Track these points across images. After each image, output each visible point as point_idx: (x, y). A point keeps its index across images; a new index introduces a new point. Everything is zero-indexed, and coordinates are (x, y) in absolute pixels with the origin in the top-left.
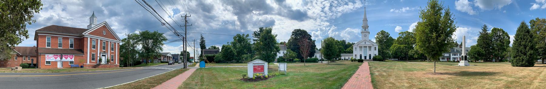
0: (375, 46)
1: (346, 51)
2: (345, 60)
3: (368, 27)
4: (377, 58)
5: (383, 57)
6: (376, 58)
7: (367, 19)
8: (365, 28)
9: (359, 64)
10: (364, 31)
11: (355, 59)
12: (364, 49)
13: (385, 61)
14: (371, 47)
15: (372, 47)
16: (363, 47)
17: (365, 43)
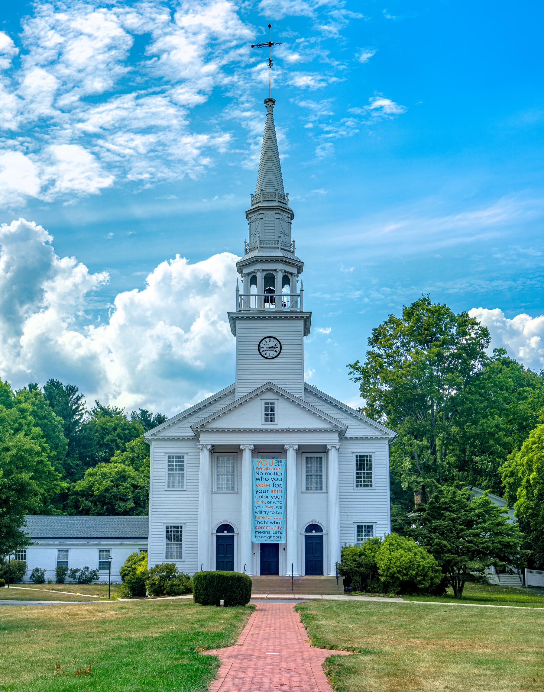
0: (362, 448)
1: (81, 485)
2: (60, 581)
3: (300, 269)
4: (382, 565)
5: (438, 552)
6: (374, 568)
7: (283, 198)
8: (270, 280)
9: (213, 627)
10: (254, 304)
11: (170, 570)
12: (256, 476)
13: (458, 596)
14: (324, 450)
15: (333, 455)
16: (247, 455)
17: (270, 417)
